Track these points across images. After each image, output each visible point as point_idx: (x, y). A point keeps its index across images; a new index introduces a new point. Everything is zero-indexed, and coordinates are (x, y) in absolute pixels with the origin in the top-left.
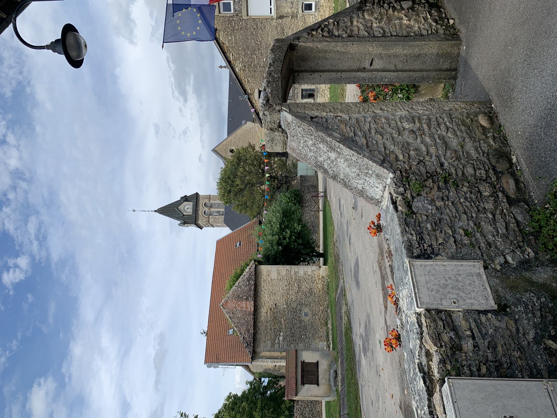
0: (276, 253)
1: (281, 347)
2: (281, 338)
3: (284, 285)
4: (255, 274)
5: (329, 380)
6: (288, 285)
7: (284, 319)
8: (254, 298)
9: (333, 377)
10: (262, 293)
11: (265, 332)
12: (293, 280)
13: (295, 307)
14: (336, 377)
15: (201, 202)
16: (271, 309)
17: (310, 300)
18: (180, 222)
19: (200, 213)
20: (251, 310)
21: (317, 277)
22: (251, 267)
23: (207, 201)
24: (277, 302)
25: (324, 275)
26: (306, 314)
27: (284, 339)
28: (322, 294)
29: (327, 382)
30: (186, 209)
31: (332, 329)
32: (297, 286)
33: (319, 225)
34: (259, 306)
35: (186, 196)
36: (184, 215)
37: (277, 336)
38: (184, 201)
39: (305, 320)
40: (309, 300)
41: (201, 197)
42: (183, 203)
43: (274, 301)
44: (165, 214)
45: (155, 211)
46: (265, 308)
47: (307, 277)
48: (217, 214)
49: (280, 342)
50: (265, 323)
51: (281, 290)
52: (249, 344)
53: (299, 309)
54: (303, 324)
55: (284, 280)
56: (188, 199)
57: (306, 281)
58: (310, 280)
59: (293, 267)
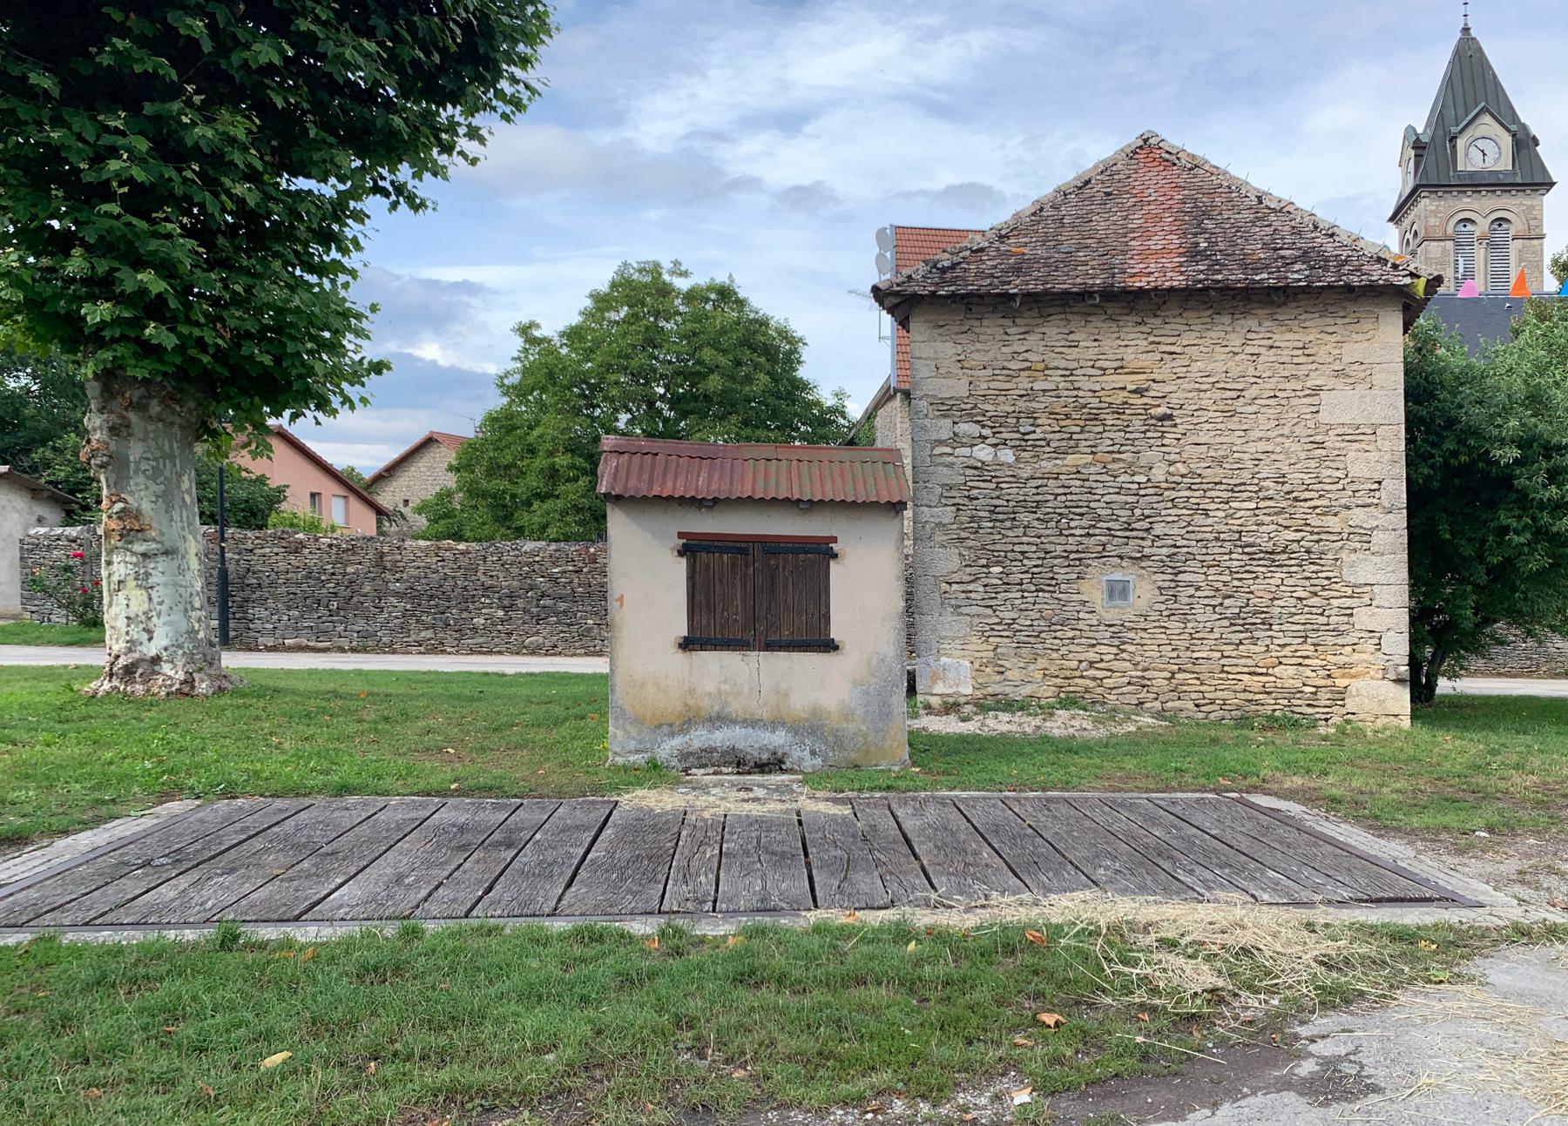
0: (1475, 433)
1: (937, 451)
2: (983, 453)
3: (1285, 469)
4: (1349, 289)
5: (719, 720)
6: (1287, 488)
7: (1085, 466)
8: (1206, 289)
9: (740, 745)
10: (1235, 341)
11: (1014, 365)
12: (1314, 521)
13: (1159, 529)
14: (741, 763)
15: (1512, 204)
16: (1139, 392)
17: (1204, 616)
18: (1420, 131)
19: (1466, 201)
20: (1134, 275)
21: (1341, 660)
22: (1395, 267)
23: (1517, 227)
24: (1181, 429)
25: (1351, 705)
26: (1117, 591)
27: (980, 468)
28: (1240, 687)
29: (708, 706)
30: (1480, 143)
31: (1046, 742)
32: (1282, 543)
33: (1500, 675)
34: (1158, 321)
35: (1536, 142)
36: (1453, 139)
37: (995, 428)
38: (1514, 136)
39: (1084, 586)
40: (1198, 609)
41: (1535, 202)
42: (1508, 130)
43: (1189, 408)
44: (1457, 63)
45: (1466, 30)
46: (1147, 360)
47: (1335, 602)
48: (1461, 270)
49: (963, 445)
50: (1063, 364)
51: (1251, 447)
52: (948, 275)
53: (1147, 551)
54: (1062, 574)
55: (1313, 464)
56: (1524, 152)
57: (1316, 594)
58: (1323, 620)
59: (1400, 520)
